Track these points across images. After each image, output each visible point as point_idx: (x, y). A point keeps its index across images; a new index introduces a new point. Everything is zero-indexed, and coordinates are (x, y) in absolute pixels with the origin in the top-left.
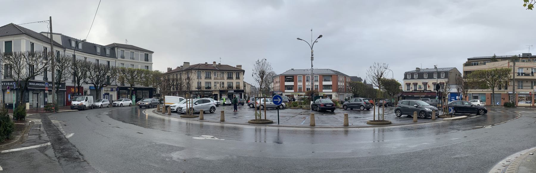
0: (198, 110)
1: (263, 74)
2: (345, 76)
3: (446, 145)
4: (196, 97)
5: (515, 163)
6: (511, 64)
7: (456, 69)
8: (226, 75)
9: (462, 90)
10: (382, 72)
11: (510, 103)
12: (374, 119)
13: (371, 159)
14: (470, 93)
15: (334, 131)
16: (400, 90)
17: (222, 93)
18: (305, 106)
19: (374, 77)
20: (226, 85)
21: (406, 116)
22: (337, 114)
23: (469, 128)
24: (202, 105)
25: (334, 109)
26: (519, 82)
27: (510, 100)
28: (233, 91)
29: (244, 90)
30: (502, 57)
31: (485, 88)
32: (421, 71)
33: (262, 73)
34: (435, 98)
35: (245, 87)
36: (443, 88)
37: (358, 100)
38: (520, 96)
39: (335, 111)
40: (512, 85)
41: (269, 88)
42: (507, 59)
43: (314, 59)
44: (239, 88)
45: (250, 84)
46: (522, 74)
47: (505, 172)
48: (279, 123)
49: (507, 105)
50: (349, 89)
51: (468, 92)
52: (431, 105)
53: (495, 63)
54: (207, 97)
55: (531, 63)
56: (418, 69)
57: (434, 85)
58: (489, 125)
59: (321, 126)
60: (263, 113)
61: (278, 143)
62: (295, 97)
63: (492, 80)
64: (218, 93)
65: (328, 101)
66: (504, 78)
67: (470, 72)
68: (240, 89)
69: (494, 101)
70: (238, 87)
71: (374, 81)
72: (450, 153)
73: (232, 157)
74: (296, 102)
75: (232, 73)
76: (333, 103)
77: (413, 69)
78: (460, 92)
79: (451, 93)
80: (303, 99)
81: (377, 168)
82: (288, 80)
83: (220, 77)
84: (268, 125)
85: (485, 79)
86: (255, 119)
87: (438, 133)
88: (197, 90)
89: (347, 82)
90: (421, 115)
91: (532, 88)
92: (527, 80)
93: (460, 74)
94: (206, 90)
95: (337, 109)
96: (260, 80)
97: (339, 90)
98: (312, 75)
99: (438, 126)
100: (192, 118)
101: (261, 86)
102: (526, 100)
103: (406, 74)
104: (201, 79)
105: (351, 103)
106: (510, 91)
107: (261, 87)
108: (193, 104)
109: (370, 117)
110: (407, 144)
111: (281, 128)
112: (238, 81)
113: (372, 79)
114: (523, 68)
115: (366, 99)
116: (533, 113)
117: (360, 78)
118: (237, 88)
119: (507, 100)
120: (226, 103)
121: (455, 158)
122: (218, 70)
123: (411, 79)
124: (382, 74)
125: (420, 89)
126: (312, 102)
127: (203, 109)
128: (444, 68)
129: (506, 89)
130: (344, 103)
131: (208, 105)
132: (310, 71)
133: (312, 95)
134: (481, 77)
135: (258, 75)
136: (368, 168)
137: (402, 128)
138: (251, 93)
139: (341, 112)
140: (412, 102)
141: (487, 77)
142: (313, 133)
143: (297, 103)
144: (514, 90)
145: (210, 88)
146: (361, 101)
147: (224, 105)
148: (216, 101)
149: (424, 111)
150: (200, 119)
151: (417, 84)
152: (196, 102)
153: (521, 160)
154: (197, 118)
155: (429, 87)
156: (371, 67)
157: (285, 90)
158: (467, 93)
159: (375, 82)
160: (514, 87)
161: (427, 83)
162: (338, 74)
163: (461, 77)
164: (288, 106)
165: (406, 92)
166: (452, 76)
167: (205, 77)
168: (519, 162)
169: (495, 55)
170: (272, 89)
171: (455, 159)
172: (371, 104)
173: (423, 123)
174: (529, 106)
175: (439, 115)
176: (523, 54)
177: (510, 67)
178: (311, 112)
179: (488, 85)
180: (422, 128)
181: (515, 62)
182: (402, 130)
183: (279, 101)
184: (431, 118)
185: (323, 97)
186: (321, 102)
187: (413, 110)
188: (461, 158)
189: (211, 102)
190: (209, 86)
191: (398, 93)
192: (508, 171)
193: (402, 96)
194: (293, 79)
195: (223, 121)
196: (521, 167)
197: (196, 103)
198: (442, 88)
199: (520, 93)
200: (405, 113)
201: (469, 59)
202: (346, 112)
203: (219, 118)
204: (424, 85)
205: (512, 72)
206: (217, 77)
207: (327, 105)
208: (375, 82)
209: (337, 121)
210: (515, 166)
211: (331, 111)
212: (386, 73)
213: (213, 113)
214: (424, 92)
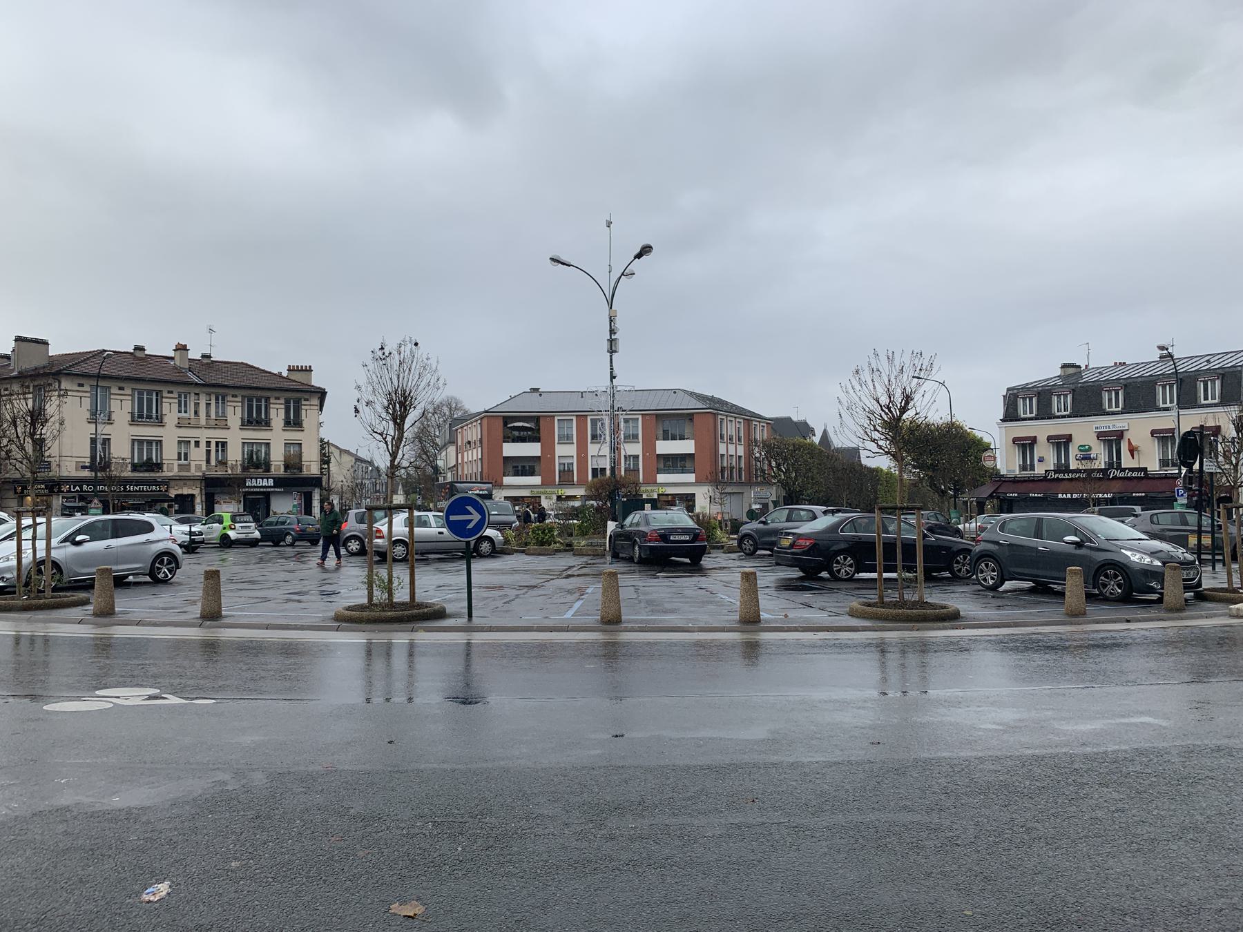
0: (87, 572)
1: (402, 404)
2: (749, 418)
4: (80, 509)
8: (239, 410)
10: (908, 390)
15: (698, 644)
16: (983, 468)
17: (219, 490)
18: (583, 543)
19: (872, 413)
20: (235, 455)
21: (1031, 584)
22: (714, 574)
24: (109, 547)
25: (702, 551)
28: (271, 482)
29: (325, 478)
32: (1087, 377)
33: (400, 403)
34: (1169, 502)
35: (328, 462)
37: (802, 513)
39: (706, 562)
41: (436, 469)
43: (621, 346)
44: (300, 469)
45: (348, 452)
48: (470, 615)
50: (763, 471)
52: (1153, 536)
54: (138, 508)
56: (1071, 371)
59: (647, 621)
60: (401, 573)
61: (466, 702)
62: (545, 503)
64: (196, 492)
65: (678, 518)
68: (305, 472)
70: (293, 463)
73: (244, 781)
74: (548, 525)
75: (267, 399)
76: (696, 526)
77: (1046, 370)
80: (575, 513)
81: (917, 818)
82: (516, 433)
83: (208, 415)
84: (421, 628)
86: (365, 601)
87: (1201, 676)
88: (86, 473)
89: (756, 441)
90: (1105, 586)
94: (137, 474)
95: (715, 553)
96: (391, 429)
97: (723, 477)
98: (613, 412)
99: (1202, 641)
100: (47, 612)
101: (394, 455)
104: (109, 421)
105: (772, 526)
107: (392, 461)
108: (54, 542)
110: (1049, 713)
111: (478, 638)
112: (293, 435)
113: (866, 423)
117: (805, 424)
118: (287, 467)
120: (233, 534)
122: (197, 384)
123: (1036, 419)
124: (908, 399)
126: (611, 526)
127: (114, 568)
130: (745, 529)
131: (143, 546)
132: (603, 399)
133: (611, 496)
135: (380, 409)
138: (356, 489)
139: (731, 564)
140: (1056, 520)
142: (611, 653)
143: (551, 530)
145: (159, 466)
147: (226, 543)
148: (186, 528)
149: (1120, 568)
150: (96, 615)
151: (1069, 438)
152: (78, 532)
154: (80, 608)
155: (1132, 451)
156: (857, 372)
157: (504, 476)
159: (876, 435)
162: (716, 409)
164: (513, 542)
165: (1015, 481)
167: (133, 414)
170: (449, 475)
175: (1204, 587)
178: (609, 566)
180: (1118, 645)
183: (470, 521)
185: (655, 504)
186: (647, 523)
187: (1059, 562)
189: (160, 532)
190: (150, 459)
191: (976, 484)
193: (998, 498)
194: (539, 429)
195: (212, 615)
197: (79, 538)
200: (1019, 570)
202: (749, 566)
203: (194, 603)
204: (1109, 444)
206: (192, 416)
207: (672, 538)
208: (876, 435)
209: (711, 603)
211: (687, 560)
213: (165, 582)
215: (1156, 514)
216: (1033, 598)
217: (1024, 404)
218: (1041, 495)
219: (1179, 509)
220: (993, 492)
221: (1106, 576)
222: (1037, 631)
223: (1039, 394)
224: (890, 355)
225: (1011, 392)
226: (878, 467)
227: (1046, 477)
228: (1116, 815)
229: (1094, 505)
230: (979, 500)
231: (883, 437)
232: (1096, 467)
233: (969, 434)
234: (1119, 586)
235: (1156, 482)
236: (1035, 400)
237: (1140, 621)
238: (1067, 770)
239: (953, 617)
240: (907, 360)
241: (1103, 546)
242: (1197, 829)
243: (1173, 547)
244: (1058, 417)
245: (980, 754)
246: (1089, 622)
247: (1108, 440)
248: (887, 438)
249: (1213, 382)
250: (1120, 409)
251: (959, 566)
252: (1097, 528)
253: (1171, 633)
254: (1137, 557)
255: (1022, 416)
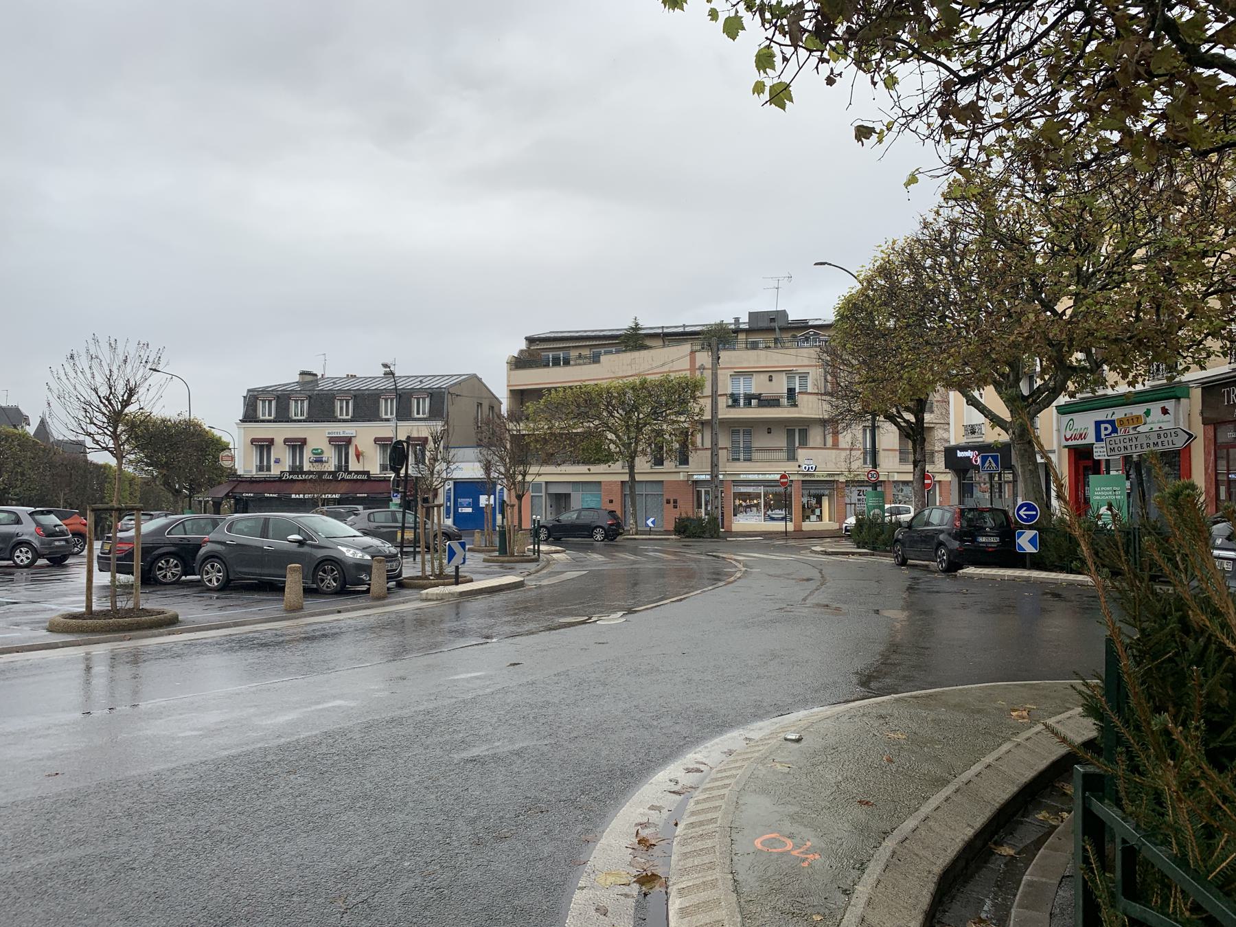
3: (431, 706)
5: (722, 778)
6: (704, 358)
7: (480, 380)
9: (502, 470)
10: (132, 383)
11: (700, 519)
12: (89, 606)
13: (62, 805)
14: (538, 479)
16: (221, 468)
23: (531, 626)
26: (735, 432)
27: (699, 506)
30: (665, 330)
31: (599, 460)
32: (323, 386)
34: (386, 502)
36: (420, 460)
38: (743, 490)
40: (708, 444)
42: (686, 340)
46: (749, 398)
47: (681, 818)
49: (687, 530)
51: (528, 478)
52: (366, 533)
53: (636, 354)
55: (783, 351)
56: (309, 378)
57: (384, 447)
58: (615, 612)
63: (628, 427)
66: (673, 417)
67: (536, 394)
69: (634, 515)
71: (92, 423)
72: (447, 737)
77: (284, 375)
78: (496, 475)
79: (458, 484)
81: (90, 850)
85: (597, 422)
87: (398, 653)
90: (322, 580)
91: (792, 457)
92: (769, 426)
93: (494, 403)
99: (398, 625)
102: (768, 506)
103: (252, 400)
106: (698, 469)
109: (65, 596)
110: (252, 710)
113: (81, 414)
114: (751, 373)
115: (49, 512)
116: (797, 560)
117: (17, 410)
119: (686, 509)
121: (467, 761)
123: (274, 421)
124: (131, 392)
125: (318, 468)
128: (426, 377)
129: (684, 461)
134: (582, 416)
136: (41, 858)
137: (230, 639)
140: (277, 519)
141: (605, 414)
144: (714, 465)
146: (18, 521)
149: (335, 562)
151: (304, 442)
153: (746, 764)
155: (358, 455)
156: (72, 357)
158: (523, 482)
159: (92, 429)
160: (714, 455)
161: (349, 441)
163: (499, 416)
165: (252, 481)
166: (463, 411)
168: (740, 772)
169: (637, 324)
171: (470, 766)
172: (74, 535)
173: (332, 612)
174: (782, 532)
175: (403, 576)
176: (750, 314)
177: (698, 373)
179: (612, 446)
180: (325, 636)
181: (718, 350)
182: (231, 649)
183: (1025, 511)
184: (368, 591)
187: (282, 559)
188: (496, 758)
191: (212, 483)
192: (693, 813)
193: (234, 498)
196: (749, 799)
198: (417, 463)
199: (742, 477)
201: (531, 340)
204: (339, 448)
205: (708, 391)
208: (92, 429)
210: (722, 792)
212: (153, 391)
214: (335, 479)
215: (373, 513)
216: (256, 596)
217: (264, 407)
218: (275, 496)
219: (393, 508)
220: (229, 493)
221: (324, 571)
222: (255, 629)
223: (278, 398)
224: (113, 343)
225: (251, 393)
226: (106, 464)
227: (281, 478)
228: (298, 799)
229: (323, 505)
230: (216, 500)
231: (101, 432)
232: (326, 470)
233: (207, 433)
234: (335, 580)
235: (376, 484)
236: (274, 403)
237: (349, 611)
238: (259, 765)
239: (170, 623)
240: (132, 350)
241: (323, 544)
242: (366, 797)
243: (383, 543)
244: (295, 421)
245: (174, 765)
246: (305, 616)
247: (338, 445)
248: (105, 433)
249: (424, 399)
250: (349, 417)
251: (164, 572)
252: (318, 527)
253: (372, 619)
254: (351, 552)
255: (261, 418)
